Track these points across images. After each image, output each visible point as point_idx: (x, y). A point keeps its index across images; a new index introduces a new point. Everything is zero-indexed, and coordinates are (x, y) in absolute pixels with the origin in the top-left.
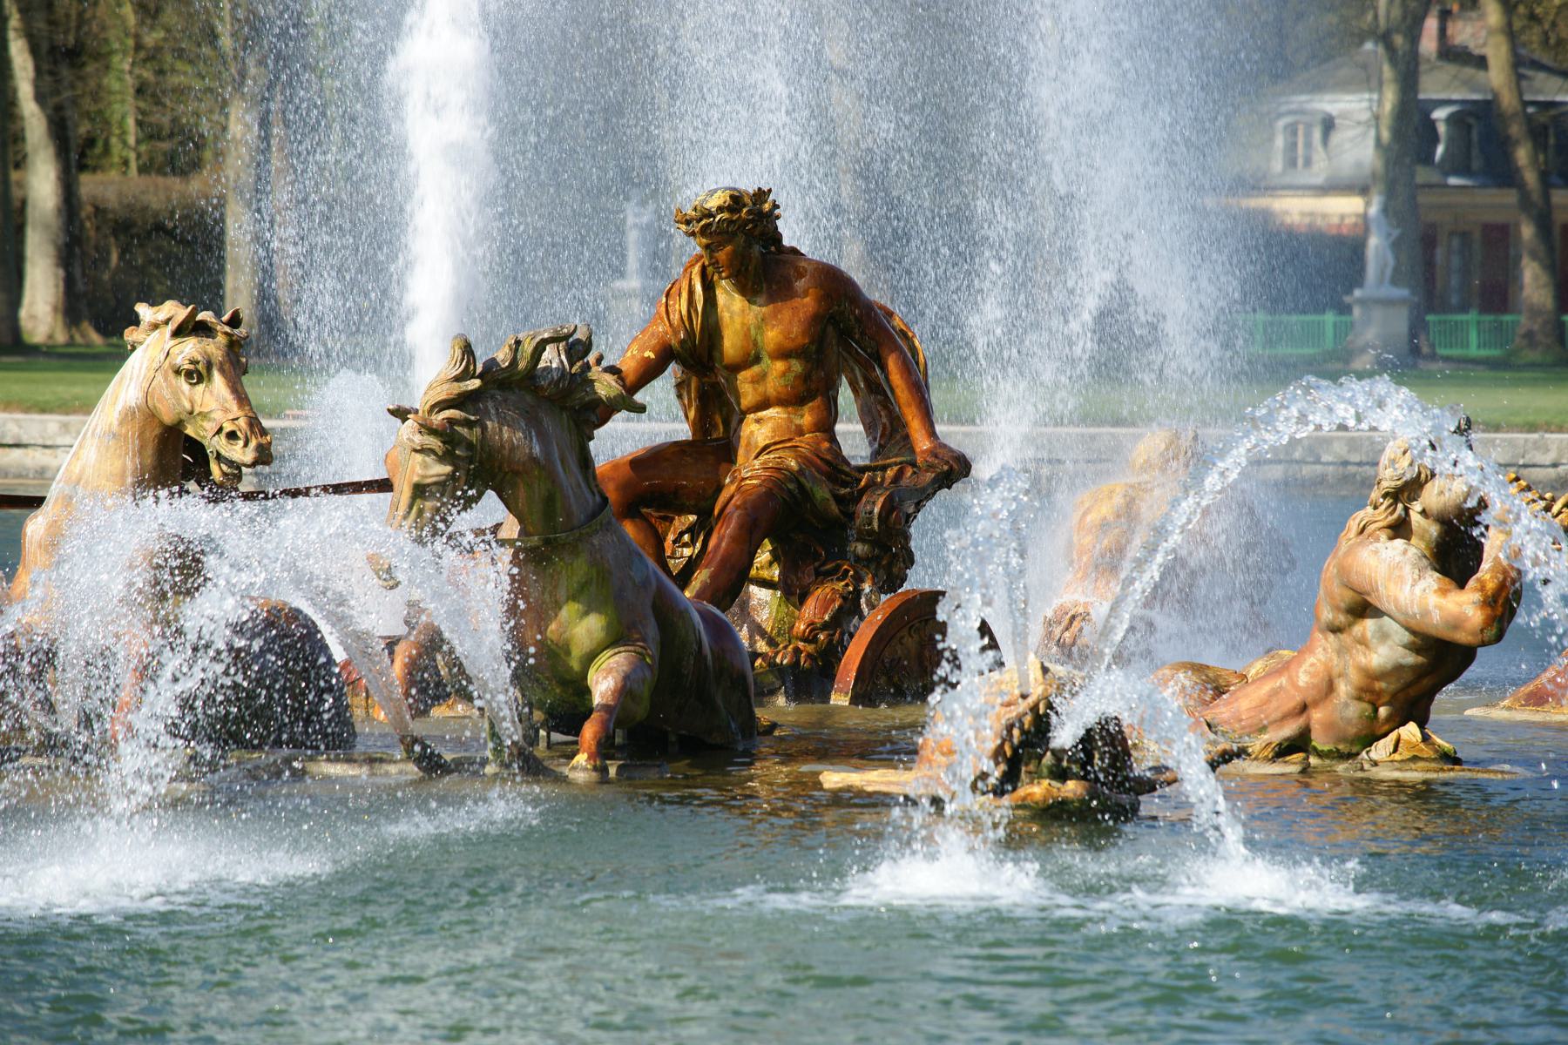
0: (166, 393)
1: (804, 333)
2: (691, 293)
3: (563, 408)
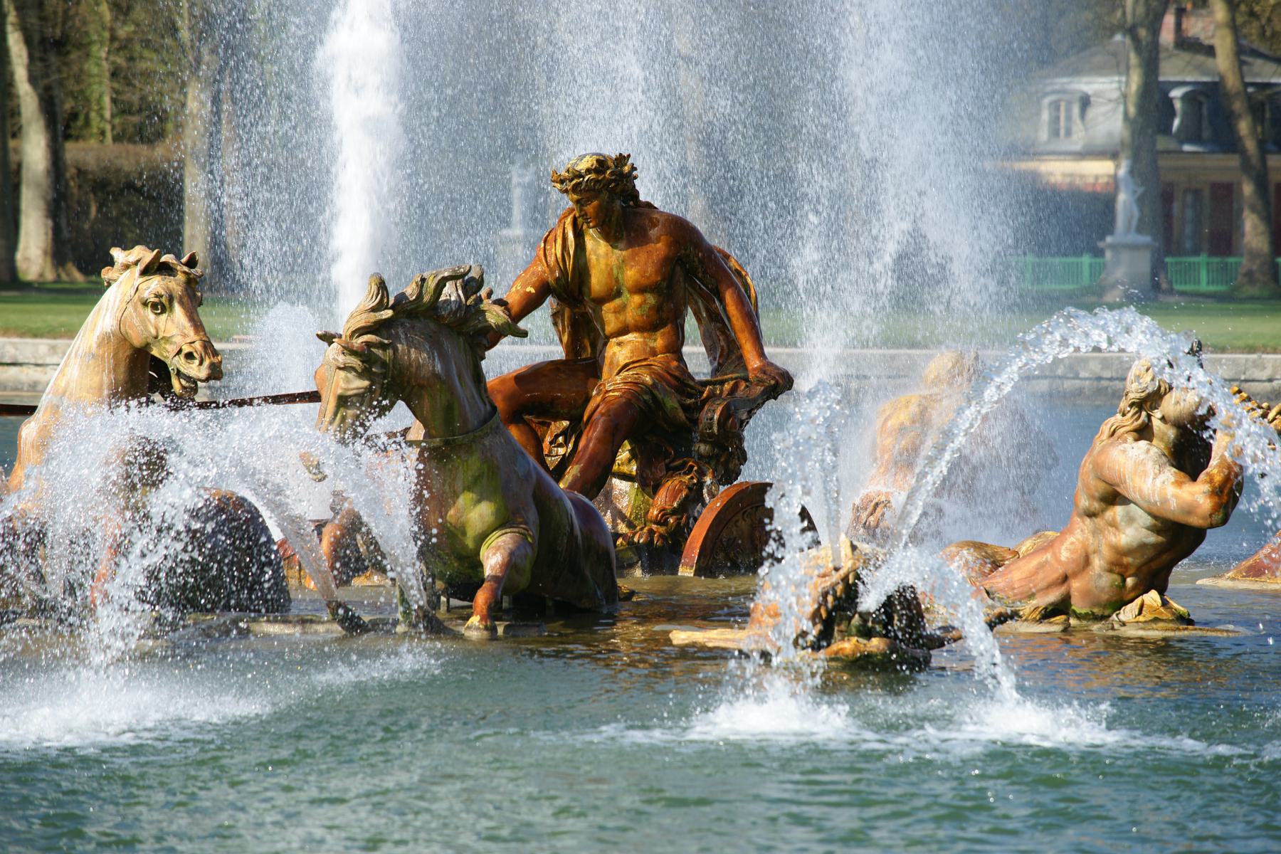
0: (136, 321)
1: (657, 272)
2: (565, 239)
3: (460, 334)
